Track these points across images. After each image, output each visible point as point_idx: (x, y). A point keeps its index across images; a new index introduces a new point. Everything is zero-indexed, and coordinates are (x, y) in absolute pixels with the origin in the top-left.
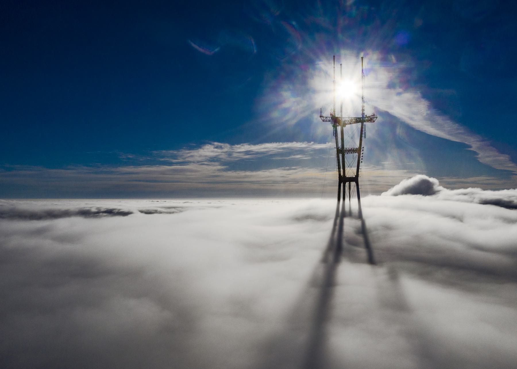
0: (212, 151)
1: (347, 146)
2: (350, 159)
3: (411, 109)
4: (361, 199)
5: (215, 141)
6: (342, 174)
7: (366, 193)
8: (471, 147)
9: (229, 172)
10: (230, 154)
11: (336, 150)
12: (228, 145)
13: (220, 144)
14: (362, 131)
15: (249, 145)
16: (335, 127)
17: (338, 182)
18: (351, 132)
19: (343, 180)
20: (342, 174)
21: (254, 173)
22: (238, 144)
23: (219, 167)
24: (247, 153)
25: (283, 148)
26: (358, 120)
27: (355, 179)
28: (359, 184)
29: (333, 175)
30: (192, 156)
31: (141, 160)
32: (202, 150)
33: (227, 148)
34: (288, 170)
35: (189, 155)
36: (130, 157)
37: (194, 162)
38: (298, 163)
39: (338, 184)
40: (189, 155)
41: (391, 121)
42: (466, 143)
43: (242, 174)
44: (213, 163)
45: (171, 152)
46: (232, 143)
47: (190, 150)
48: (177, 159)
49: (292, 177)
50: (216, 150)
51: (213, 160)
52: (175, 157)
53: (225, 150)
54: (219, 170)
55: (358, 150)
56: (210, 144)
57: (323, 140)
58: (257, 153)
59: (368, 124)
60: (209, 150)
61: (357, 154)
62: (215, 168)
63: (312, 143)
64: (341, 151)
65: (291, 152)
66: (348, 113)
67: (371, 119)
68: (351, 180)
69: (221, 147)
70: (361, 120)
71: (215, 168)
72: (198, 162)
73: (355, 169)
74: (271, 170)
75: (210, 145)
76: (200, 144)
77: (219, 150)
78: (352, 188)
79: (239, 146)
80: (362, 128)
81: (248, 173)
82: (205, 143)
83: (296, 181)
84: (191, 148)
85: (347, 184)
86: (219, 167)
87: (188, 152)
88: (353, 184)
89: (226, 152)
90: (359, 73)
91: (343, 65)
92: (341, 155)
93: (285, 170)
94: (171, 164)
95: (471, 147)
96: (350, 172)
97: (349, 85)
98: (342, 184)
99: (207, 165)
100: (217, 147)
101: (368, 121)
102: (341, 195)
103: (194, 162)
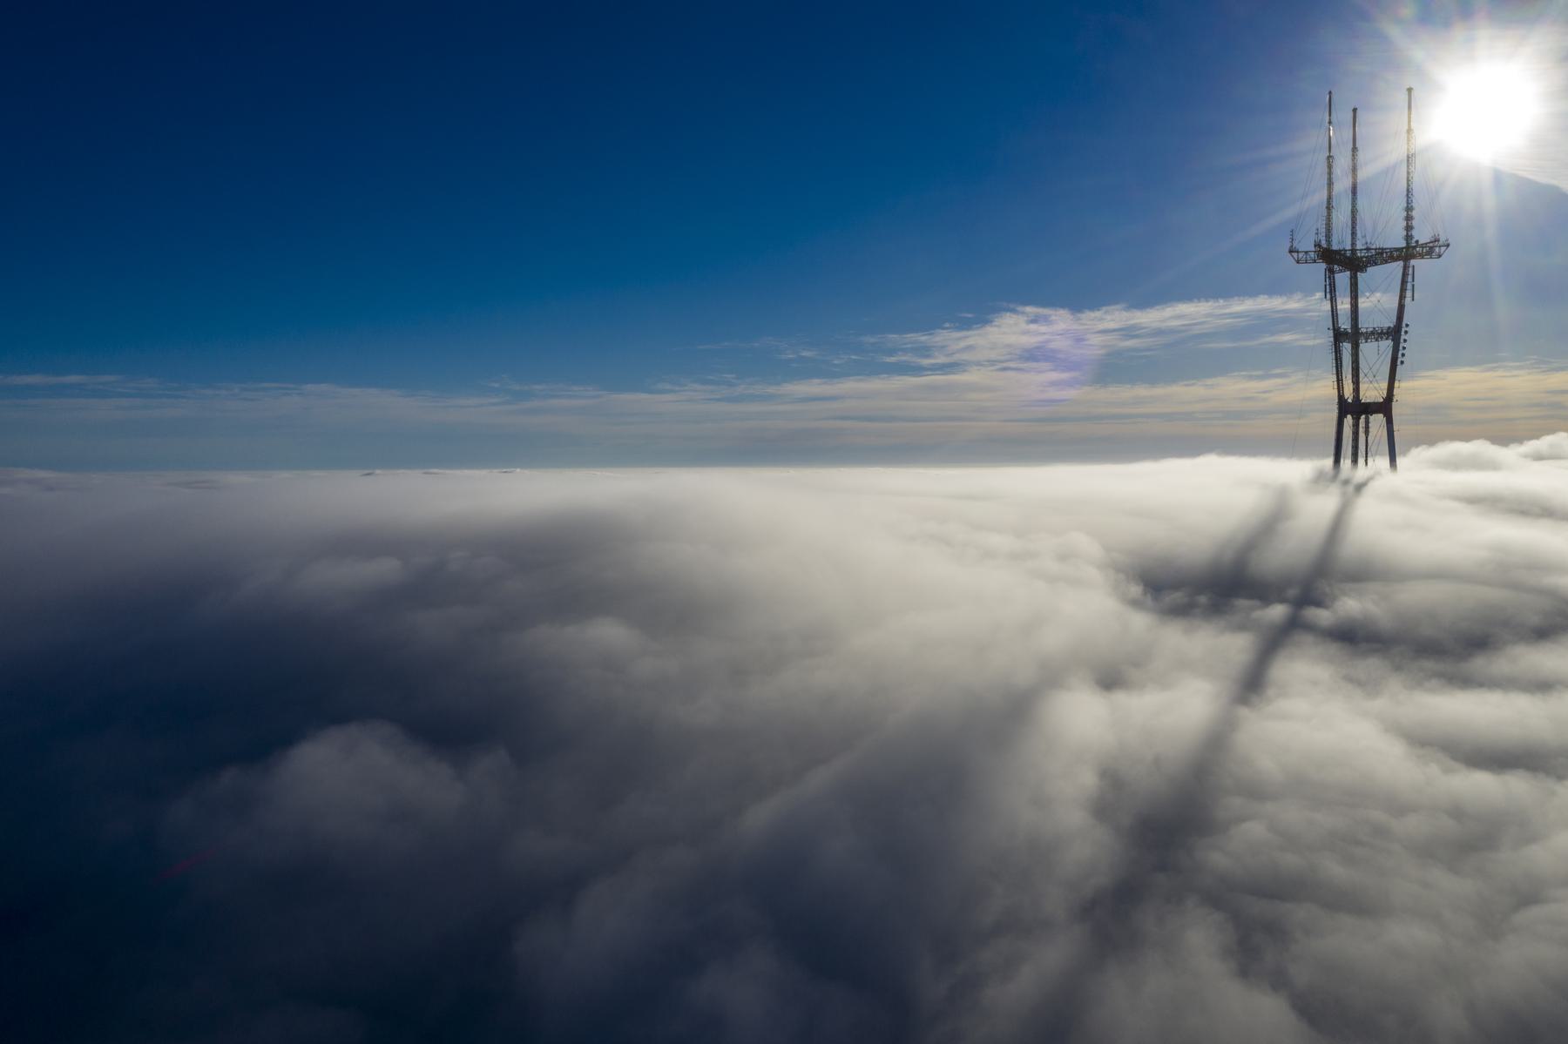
0: (1025, 333)
2: (1374, 354)
15: (1128, 309)
19: (1353, 409)
20: (1348, 393)
21: (1159, 391)
23: (1055, 376)
36: (805, 354)
37: (979, 364)
40: (962, 344)
44: (1034, 365)
47: (960, 329)
48: (928, 356)
50: (1033, 327)
51: (1033, 355)
54: (1054, 384)
56: (1013, 311)
58: (1159, 332)
60: (1013, 330)
61: (1389, 343)
69: (1045, 320)
72: (992, 362)
74: (1209, 382)
76: (982, 316)
77: (1043, 329)
81: (1142, 391)
84: (966, 325)
86: (1055, 376)
93: (1251, 378)
100: (1034, 321)
103: (979, 364)
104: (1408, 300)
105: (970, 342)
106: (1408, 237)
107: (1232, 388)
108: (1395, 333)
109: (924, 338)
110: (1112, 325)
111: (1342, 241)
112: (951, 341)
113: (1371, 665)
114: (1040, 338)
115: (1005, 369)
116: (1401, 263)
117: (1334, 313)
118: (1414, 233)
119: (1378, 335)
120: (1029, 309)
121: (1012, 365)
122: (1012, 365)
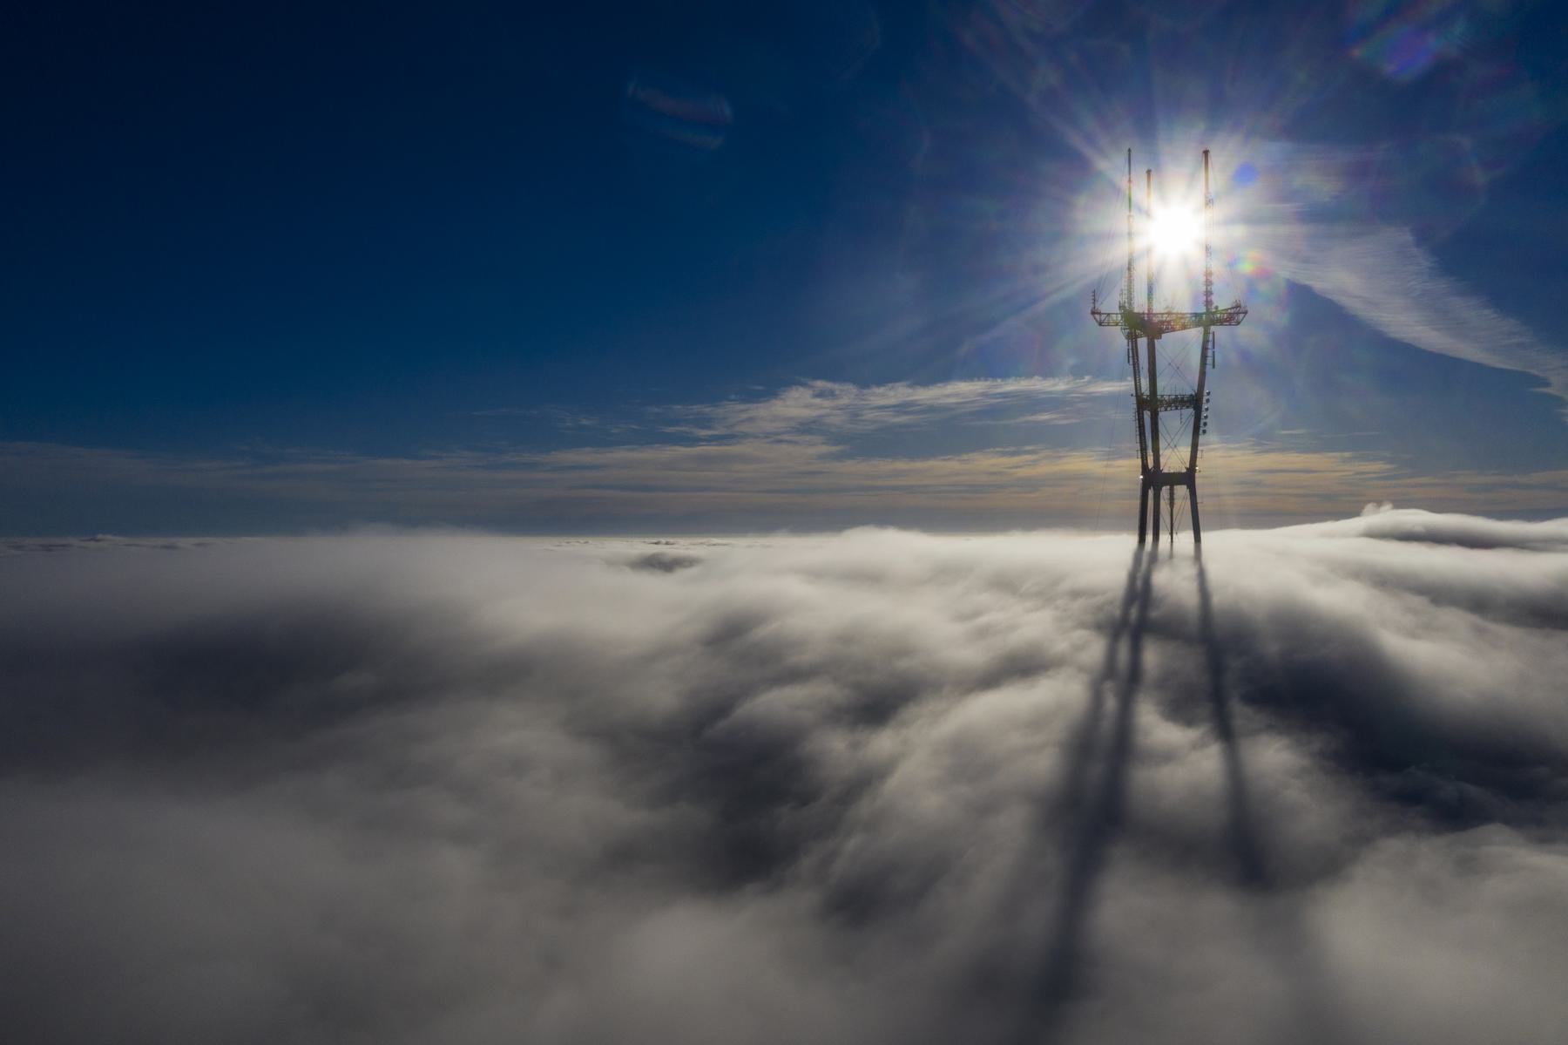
0: (806, 406)
1: (1165, 387)
2: (1174, 423)
3: (1376, 282)
4: (1204, 535)
5: (816, 378)
6: (1151, 464)
7: (1225, 520)
8: (1547, 384)
9: (850, 462)
10: (855, 414)
11: (1134, 400)
12: (851, 389)
13: (829, 385)
14: (1204, 349)
15: (910, 386)
16: (1132, 338)
17: (1139, 487)
18: (1182, 347)
19: (1154, 479)
20: (1151, 464)
21: (918, 465)
22: (879, 384)
23: (825, 449)
24: (902, 408)
25: (1005, 395)
26: (1197, 319)
27: (1188, 478)
28: (1198, 492)
29: (1129, 468)
30: (751, 419)
31: (615, 431)
32: (779, 403)
33: (847, 394)
34: (1013, 454)
35: (744, 416)
36: (584, 422)
37: (755, 436)
38: (1061, 439)
39: (1139, 493)
40: (744, 416)
41: (1313, 313)
42: (1534, 372)
43: (884, 466)
44: (808, 438)
45: (697, 408)
46: (864, 383)
47: (744, 401)
48: (709, 428)
49: (1023, 472)
50: (818, 401)
51: (807, 428)
52: (705, 422)
53: (844, 401)
54: (822, 457)
55: (1195, 402)
56: (804, 385)
57: (1101, 373)
58: (932, 409)
59: (1219, 332)
60: (797, 403)
61: (1191, 411)
62: (812, 451)
63: (1087, 378)
64: (1148, 406)
65: (1033, 403)
66: (1176, 297)
67: (1233, 316)
68: (1174, 479)
69: (832, 394)
70: (1209, 319)
71: (812, 451)
72: (767, 435)
73: (1185, 452)
74: (965, 457)
75: (801, 389)
76: (771, 390)
77: (826, 403)
78: (1178, 503)
79: (881, 390)
80: (1205, 342)
81: (901, 465)
82: (789, 383)
83: (1031, 484)
84: (752, 397)
85: (1165, 490)
86: (825, 449)
87: (742, 407)
88: (1181, 491)
89: (843, 408)
90: (1198, 197)
91: (1211, 154)
92: (1147, 415)
93: (1004, 454)
94: (695, 441)
95: (1547, 384)
96: (1174, 459)
97: (1177, 223)
98: (1151, 493)
99: (790, 442)
100: (820, 395)
101: (1221, 322)
102: (1147, 523)
103: (755, 436)
104: (1209, 368)
105: (64, 542)
106: (1208, 303)
107: (985, 463)
108: (1195, 402)
109: (707, 410)
110: (892, 401)
111: (1140, 305)
112: (737, 413)
113: (1455, 817)
114: (822, 412)
115: (780, 441)
116: (1201, 329)
117: (1137, 387)
118: (1213, 298)
119: (1179, 402)
120: (820, 384)
121: (786, 437)
122: (786, 437)
